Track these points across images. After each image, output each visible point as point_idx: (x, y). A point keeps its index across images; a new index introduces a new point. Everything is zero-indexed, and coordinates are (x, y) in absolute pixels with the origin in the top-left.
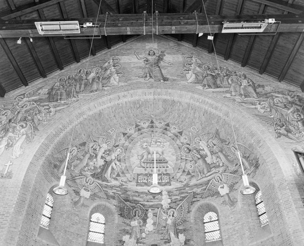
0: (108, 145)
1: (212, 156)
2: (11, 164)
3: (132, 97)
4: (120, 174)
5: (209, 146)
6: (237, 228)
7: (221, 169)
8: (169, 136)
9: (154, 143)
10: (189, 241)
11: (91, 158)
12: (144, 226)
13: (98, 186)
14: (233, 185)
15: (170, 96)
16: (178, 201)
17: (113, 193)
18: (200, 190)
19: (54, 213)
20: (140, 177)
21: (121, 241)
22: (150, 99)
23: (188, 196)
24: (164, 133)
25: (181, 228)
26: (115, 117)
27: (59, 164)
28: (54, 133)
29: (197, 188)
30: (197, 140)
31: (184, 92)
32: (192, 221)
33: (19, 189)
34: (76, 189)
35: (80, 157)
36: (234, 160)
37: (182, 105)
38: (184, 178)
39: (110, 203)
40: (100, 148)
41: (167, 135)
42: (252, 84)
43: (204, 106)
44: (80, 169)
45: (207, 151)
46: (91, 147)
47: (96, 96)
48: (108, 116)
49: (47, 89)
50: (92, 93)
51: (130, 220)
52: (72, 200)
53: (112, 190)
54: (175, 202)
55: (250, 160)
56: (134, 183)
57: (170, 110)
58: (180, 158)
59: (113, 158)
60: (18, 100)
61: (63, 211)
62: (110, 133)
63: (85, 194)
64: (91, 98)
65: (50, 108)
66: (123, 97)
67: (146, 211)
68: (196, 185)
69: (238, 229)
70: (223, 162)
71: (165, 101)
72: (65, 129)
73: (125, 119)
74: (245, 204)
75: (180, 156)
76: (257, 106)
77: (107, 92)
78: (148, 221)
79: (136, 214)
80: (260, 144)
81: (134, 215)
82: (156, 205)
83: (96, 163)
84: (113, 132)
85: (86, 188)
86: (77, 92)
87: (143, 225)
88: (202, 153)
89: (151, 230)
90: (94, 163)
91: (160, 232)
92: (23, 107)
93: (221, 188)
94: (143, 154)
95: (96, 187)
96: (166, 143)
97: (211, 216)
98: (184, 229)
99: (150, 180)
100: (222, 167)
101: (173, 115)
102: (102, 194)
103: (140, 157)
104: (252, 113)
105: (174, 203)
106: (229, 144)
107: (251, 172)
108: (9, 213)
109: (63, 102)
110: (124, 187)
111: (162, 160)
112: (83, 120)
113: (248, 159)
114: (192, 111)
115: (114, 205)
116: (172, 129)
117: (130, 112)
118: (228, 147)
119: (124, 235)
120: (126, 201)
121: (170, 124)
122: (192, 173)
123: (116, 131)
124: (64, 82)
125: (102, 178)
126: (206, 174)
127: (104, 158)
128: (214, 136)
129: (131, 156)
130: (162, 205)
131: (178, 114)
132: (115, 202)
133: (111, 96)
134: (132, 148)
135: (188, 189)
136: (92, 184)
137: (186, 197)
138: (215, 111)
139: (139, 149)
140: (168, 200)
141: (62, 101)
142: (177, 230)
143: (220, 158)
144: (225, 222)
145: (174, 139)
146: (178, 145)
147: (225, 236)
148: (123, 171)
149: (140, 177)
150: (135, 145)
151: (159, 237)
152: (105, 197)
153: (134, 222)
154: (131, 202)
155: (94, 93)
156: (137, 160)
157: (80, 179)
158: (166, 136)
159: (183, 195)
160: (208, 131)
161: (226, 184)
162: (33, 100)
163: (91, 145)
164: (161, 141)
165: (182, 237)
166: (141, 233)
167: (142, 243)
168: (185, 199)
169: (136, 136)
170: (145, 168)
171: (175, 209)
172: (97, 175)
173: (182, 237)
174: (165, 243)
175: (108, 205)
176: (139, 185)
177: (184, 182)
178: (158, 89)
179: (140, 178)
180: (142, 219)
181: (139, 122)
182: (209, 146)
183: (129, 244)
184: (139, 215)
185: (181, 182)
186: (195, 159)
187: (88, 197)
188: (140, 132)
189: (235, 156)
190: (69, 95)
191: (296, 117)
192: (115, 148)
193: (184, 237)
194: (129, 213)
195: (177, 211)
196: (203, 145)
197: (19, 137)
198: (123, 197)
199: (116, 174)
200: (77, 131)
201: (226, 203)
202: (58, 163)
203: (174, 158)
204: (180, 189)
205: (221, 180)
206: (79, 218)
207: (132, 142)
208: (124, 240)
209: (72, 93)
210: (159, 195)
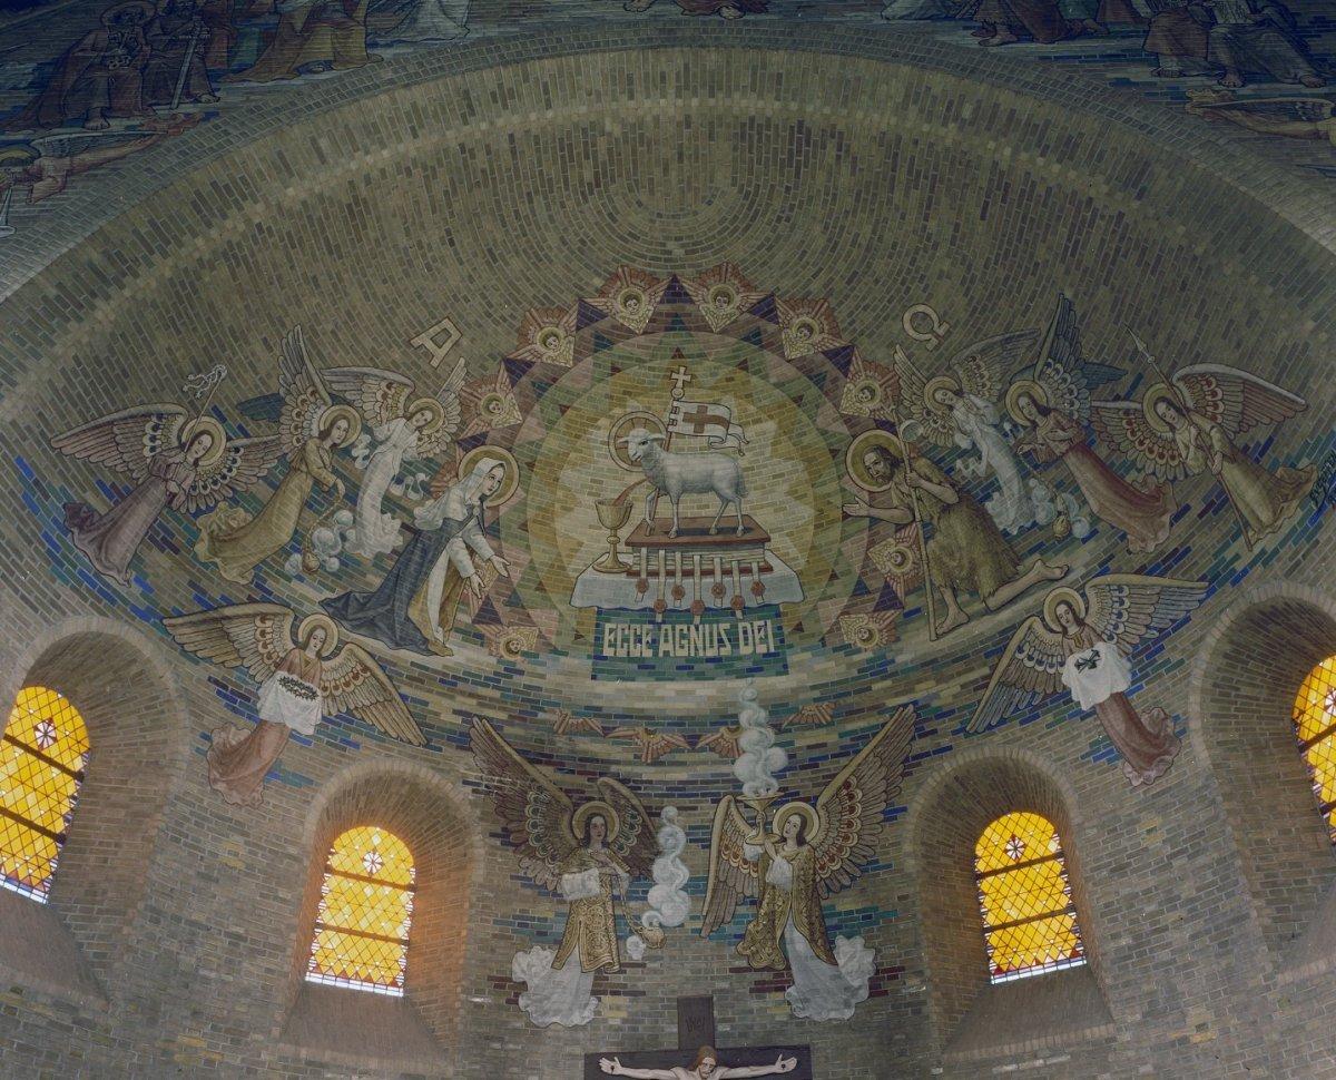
0: (419, 429)
1: (1026, 485)
4: (499, 607)
5: (1011, 420)
6: (1187, 890)
7: (1081, 559)
8: (773, 380)
9: (690, 428)
10: (896, 977)
11: (320, 500)
12: (637, 899)
13: (366, 669)
14: (1157, 640)
15: (778, 91)
16: (826, 758)
17: (456, 712)
18: (958, 689)
19: (90, 811)
20: (613, 626)
22: (656, 119)
23: (883, 725)
24: (743, 366)
25: (846, 904)
26: (452, 243)
27: (103, 510)
29: (938, 682)
30: (939, 396)
31: (862, 63)
32: (911, 865)
35: (253, 489)
36: (1169, 489)
37: (855, 159)
38: (863, 626)
40: (373, 445)
41: (765, 377)
42: (1276, 17)
43: (992, 145)
44: (255, 560)
46: (315, 433)
47: (327, 92)
48: (407, 231)
49: (31, 66)
52: (207, 738)
53: (452, 698)
54: (813, 764)
55: (1275, 464)
56: (580, 662)
57: (777, 204)
58: (839, 513)
59: (457, 512)
61: (143, 800)
62: (429, 356)
63: (292, 711)
64: (293, 104)
65: (33, 159)
67: (651, 815)
69: (1194, 894)
70: (1092, 514)
72: (124, 275)
73: (516, 264)
74: (1232, 742)
75: (837, 500)
76: (1321, 126)
77: (396, 72)
78: (658, 868)
79: (593, 833)
81: (580, 835)
82: (702, 782)
83: (351, 534)
85: (295, 677)
86: (212, 77)
87: (631, 896)
88: (965, 472)
89: (676, 922)
90: (343, 538)
91: (730, 929)
93: (1078, 665)
94: (625, 494)
95: (356, 677)
96: (758, 427)
97: (1018, 832)
98: (864, 910)
99: (669, 647)
100: (1085, 540)
101: (797, 236)
102: (394, 721)
103: (609, 514)
104: (1298, 161)
105: (803, 767)
106: (1134, 387)
107: (1282, 544)
109: (117, 125)
110: (525, 680)
111: (735, 530)
112: (244, 235)
113: (1266, 461)
114: (915, 194)
115: (466, 783)
116: (793, 332)
117: (542, 215)
118: (1127, 412)
119: (526, 949)
120: (532, 762)
121: (779, 304)
122: (906, 594)
123: (465, 342)
124: (138, 29)
125: (392, 629)
126: (992, 594)
127: (404, 509)
128: (1045, 352)
129: (557, 506)
130: (737, 781)
131: (826, 228)
132: (469, 764)
133: (419, 94)
134: (562, 458)
135: (885, 690)
136: (335, 654)
137: (874, 735)
138: (1056, 168)
139: (605, 462)
140: (770, 751)
141: (113, 122)
142: (823, 917)
143: (1078, 488)
144: (1110, 855)
145: (801, 398)
146: (823, 433)
147: (1115, 937)
148: (514, 592)
149: (613, 626)
150: (578, 437)
151: (721, 957)
152: (412, 732)
153: (578, 876)
154: (560, 767)
155: (316, 77)
156: (591, 527)
157: (258, 623)
158: (754, 379)
160: (1010, 324)
161: (1111, 638)
163: (318, 419)
164: (727, 417)
165: (853, 957)
166: (618, 938)
167: (626, 994)
168: (870, 746)
169: (586, 383)
170: (637, 574)
171: (812, 801)
172: (362, 607)
173: (854, 957)
174: (759, 991)
175: (427, 775)
176: (609, 672)
177: (859, 651)
178: (704, 52)
179: (611, 631)
180: (625, 859)
181: (602, 293)
182: (1007, 426)
183: (547, 998)
184: (610, 839)
185: (848, 649)
187: (311, 731)
188: (604, 356)
189: (1173, 458)
190: (158, 88)
192: (467, 451)
193: (869, 957)
194: (555, 825)
195: (822, 813)
196: (973, 423)
198: (516, 736)
199: (476, 605)
200: (211, 305)
201: (1111, 751)
202: (97, 502)
203: (806, 512)
204: (839, 689)
205: (1080, 622)
206: (246, 843)
207: (562, 422)
208: (518, 976)
210: (723, 729)
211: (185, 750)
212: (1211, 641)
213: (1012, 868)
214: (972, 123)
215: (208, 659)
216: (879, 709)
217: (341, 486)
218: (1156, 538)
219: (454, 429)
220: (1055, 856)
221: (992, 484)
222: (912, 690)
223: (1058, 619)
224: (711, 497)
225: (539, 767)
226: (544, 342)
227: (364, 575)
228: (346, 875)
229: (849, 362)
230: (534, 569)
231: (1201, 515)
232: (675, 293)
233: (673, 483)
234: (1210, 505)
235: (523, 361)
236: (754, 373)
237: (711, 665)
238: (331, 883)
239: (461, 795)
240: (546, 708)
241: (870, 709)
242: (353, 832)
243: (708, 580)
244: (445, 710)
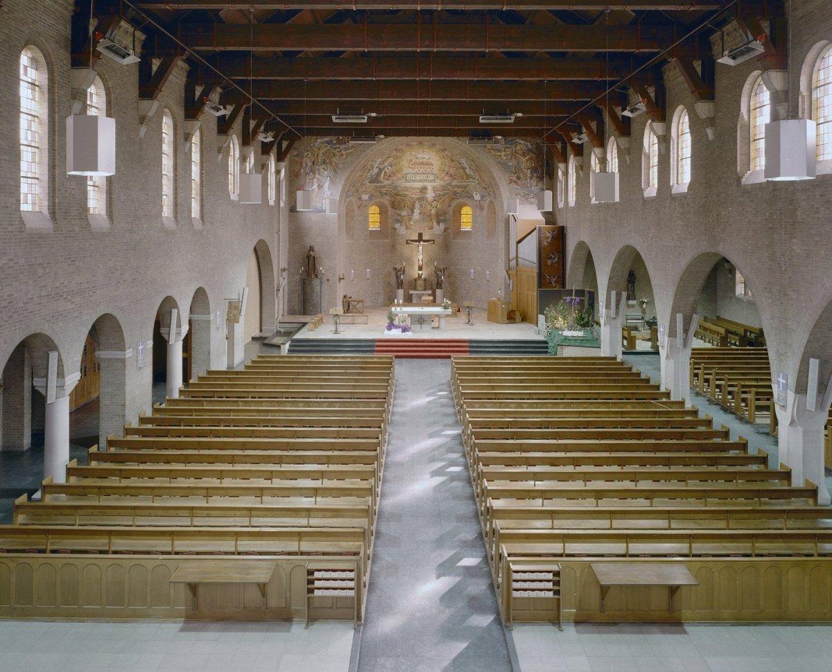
56: (404, 181)
63: (365, 197)
78: (415, 210)
102: (376, 194)
162: (326, 142)
173: (442, 226)
203: (440, 163)
216: (449, 190)
244: (384, 191)
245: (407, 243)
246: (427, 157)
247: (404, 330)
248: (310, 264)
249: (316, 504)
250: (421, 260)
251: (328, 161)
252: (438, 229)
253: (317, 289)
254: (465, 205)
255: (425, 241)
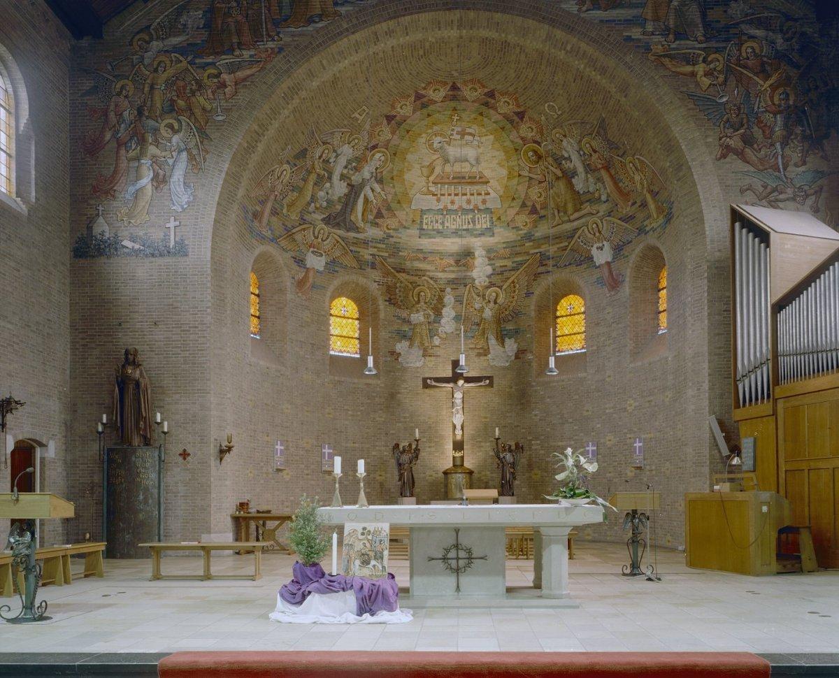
2: (177, 223)
3: (407, 34)
4: (384, 212)
5: (583, 151)
6: (614, 334)
7: (603, 208)
9: (459, 137)
11: (320, 181)
13: (338, 242)
21: (393, 353)
24: (481, 114)
25: (510, 327)
28: (246, 145)
30: (557, 135)
31: (531, 21)
33: (209, 279)
34: (298, 254)
39: (366, 278)
40: (337, 157)
41: (490, 119)
45: (577, 163)
50: (313, 25)
51: (407, 312)
53: (368, 249)
57: (496, 61)
58: (516, 174)
59: (367, 175)
60: (140, 46)
61: (280, 303)
62: (357, 119)
63: (316, 262)
66: (387, 35)
68: (546, 238)
70: (608, 193)
71: (484, 41)
73: (391, 83)
75: (516, 169)
76: (696, 68)
78: (444, 311)
80: (681, 174)
83: (330, 192)
84: (364, 115)
88: (565, 166)
90: (327, 193)
92: (157, 68)
93: (597, 248)
94: (432, 163)
98: (516, 329)
100: (605, 202)
102: (348, 261)
103: (425, 171)
105: (498, 274)
106: (624, 154)
108: (205, 324)
110: (394, 240)
115: (375, 282)
119: (400, 342)
120: (397, 272)
122: (541, 209)
123: (371, 112)
126: (571, 215)
127: (348, 178)
128: (595, 131)
132: (376, 275)
133: (358, 36)
136: (327, 238)
138: (599, 77)
141: (244, 52)
150: (414, 142)
152: (355, 264)
153: (416, 315)
158: (485, 119)
159: (519, 259)
162: (176, 49)
170: (436, 195)
171: (500, 287)
173: (511, 346)
175: (362, 281)
181: (425, 89)
182: (582, 153)
185: (517, 228)
186: (550, 178)
188: (425, 111)
191: (777, 102)
196: (569, 148)
197: (173, 157)
199: (375, 211)
203: (504, 172)
205: (600, 232)
209: (264, 26)
211: (288, 284)
212: (636, 251)
213: (568, 316)
214: (570, 52)
215: (290, 250)
216: (527, 253)
217: (326, 175)
218: (626, 209)
219: (366, 144)
220: (583, 313)
221: (575, 172)
222: (540, 248)
223: (593, 229)
224: (467, 164)
225: (400, 274)
226: (401, 108)
227: (334, 206)
228: (337, 316)
229: (524, 117)
230: (396, 195)
231: (639, 206)
232: (454, 88)
233: (451, 158)
234: (642, 204)
235: (393, 116)
236: (486, 117)
237: (465, 232)
238: (332, 319)
239: (374, 287)
240: (403, 250)
241: (524, 253)
242: (336, 300)
243: (465, 197)
245: (426, 386)
246: (471, 153)
247: (371, 601)
248: (127, 409)
249: (534, 518)
250: (459, 427)
251: (181, 103)
252: (501, 354)
253: (149, 477)
254: (568, 289)
255: (468, 380)
